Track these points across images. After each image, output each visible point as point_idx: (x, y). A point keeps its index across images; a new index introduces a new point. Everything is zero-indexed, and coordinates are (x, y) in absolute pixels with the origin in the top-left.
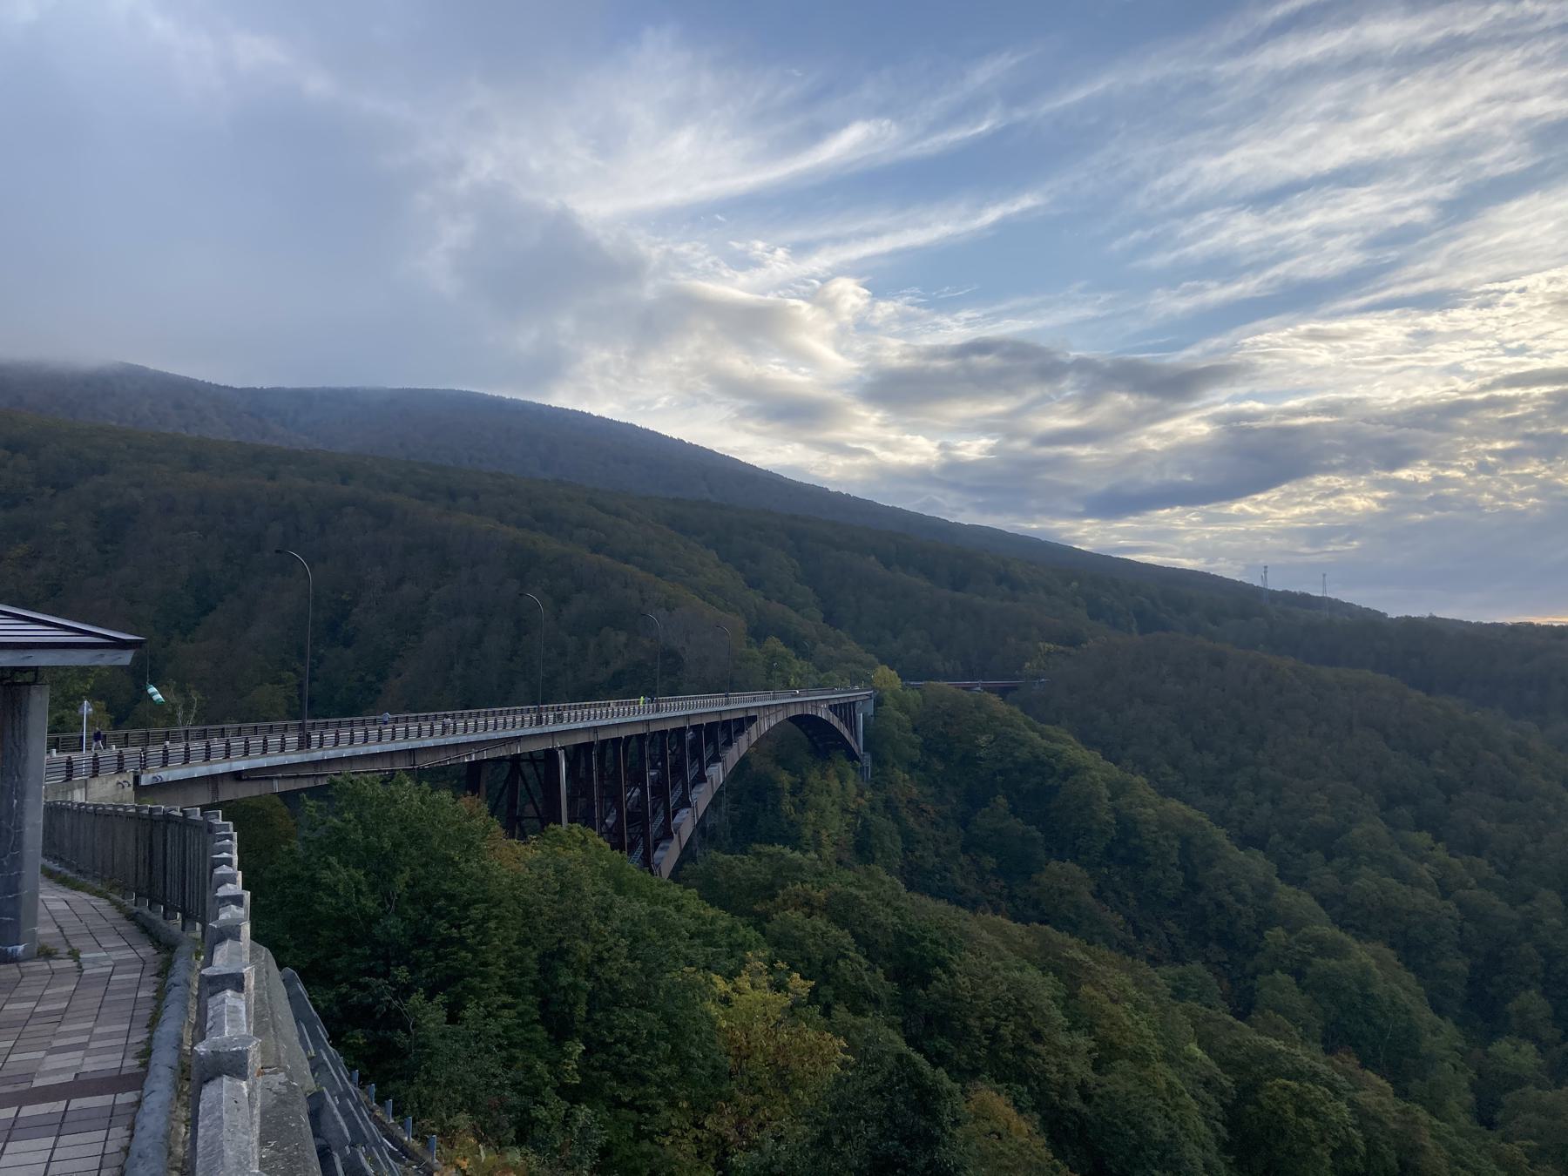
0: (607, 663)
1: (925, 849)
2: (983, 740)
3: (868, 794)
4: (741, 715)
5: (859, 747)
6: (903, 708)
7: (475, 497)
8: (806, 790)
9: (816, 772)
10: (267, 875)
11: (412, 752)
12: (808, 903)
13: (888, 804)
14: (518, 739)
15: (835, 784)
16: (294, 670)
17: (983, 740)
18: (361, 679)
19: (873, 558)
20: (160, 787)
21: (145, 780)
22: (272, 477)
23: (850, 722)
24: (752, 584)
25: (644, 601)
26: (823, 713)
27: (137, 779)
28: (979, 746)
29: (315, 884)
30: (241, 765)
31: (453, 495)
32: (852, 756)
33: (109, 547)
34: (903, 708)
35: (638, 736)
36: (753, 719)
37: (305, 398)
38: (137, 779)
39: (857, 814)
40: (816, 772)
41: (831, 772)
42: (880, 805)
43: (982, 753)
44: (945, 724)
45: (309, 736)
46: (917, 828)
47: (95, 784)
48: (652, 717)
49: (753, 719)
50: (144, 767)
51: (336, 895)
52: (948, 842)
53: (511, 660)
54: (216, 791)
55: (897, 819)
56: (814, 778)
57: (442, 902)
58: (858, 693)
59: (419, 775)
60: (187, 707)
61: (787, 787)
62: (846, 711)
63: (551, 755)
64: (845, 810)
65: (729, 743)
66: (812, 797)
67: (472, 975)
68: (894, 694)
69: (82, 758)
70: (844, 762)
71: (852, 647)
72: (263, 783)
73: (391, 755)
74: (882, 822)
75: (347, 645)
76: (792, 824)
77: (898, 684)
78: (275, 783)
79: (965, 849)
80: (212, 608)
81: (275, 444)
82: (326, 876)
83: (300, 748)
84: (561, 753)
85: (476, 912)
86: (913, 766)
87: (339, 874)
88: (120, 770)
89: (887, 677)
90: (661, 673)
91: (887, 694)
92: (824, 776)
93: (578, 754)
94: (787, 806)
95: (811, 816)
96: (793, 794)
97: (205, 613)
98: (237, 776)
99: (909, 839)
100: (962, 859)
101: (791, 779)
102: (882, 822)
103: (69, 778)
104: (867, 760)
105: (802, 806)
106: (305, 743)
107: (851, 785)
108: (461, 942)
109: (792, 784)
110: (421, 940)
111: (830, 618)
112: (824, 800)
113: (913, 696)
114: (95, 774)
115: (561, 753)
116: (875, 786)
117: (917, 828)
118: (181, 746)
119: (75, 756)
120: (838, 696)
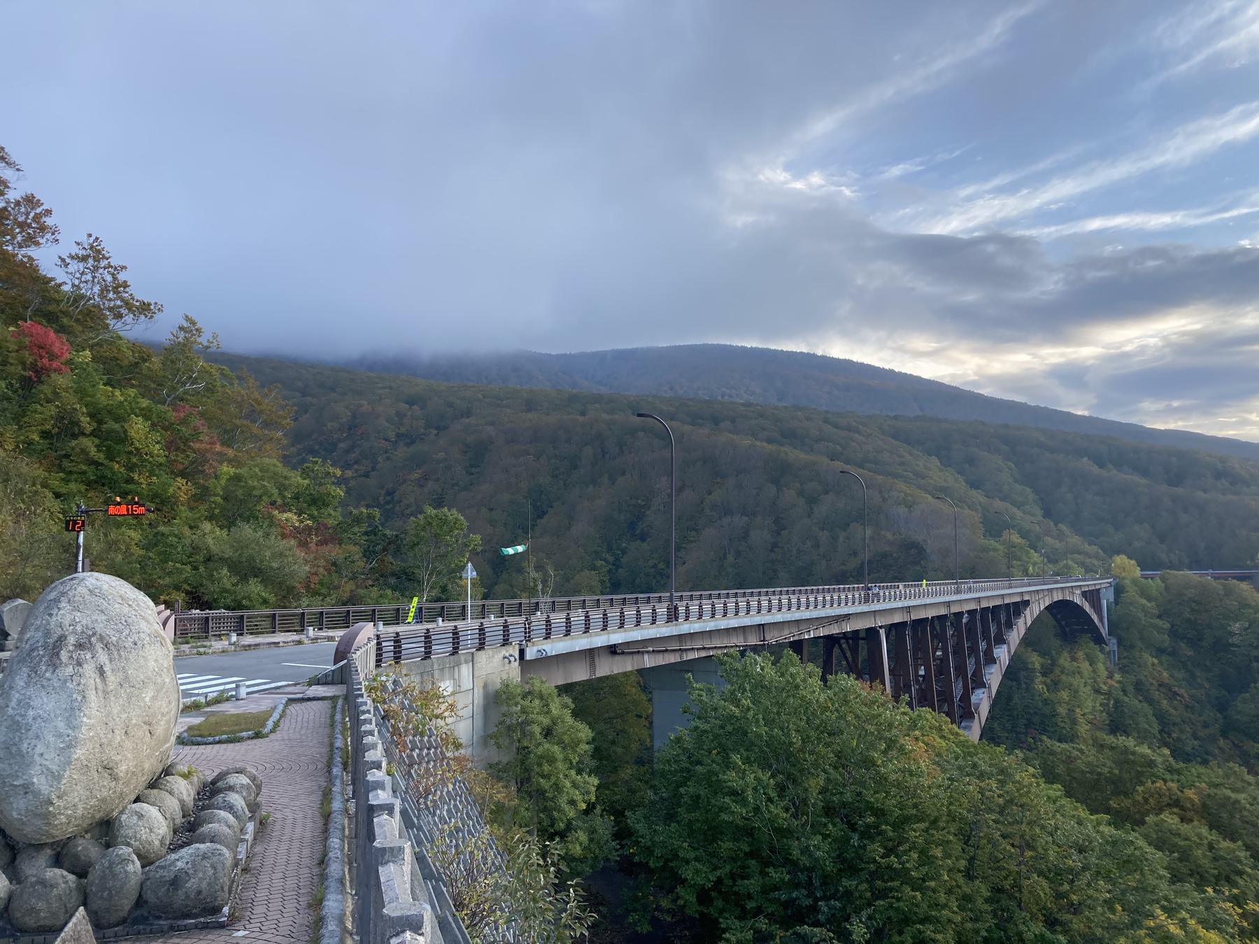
0: (855, 554)
1: (1182, 732)
2: (1236, 627)
3: (1117, 677)
4: (1018, 599)
5: (1104, 631)
6: (1143, 593)
7: (733, 421)
8: (1057, 671)
9: (1066, 654)
10: (869, 894)
11: (761, 627)
12: (1176, 803)
13: (1138, 686)
14: (847, 617)
15: (1085, 666)
16: (605, 560)
17: (1236, 627)
18: (655, 566)
19: (1085, 459)
20: (546, 661)
21: (530, 654)
22: (583, 414)
23: (1097, 607)
24: (975, 485)
25: (884, 500)
26: (1078, 600)
27: (522, 652)
28: (1232, 634)
29: (717, 787)
30: (617, 638)
31: (716, 421)
32: (1099, 640)
33: (473, 470)
34: (1143, 593)
35: (939, 617)
36: (1027, 603)
37: (600, 358)
38: (522, 652)
39: (1108, 694)
40: (1066, 654)
41: (1080, 654)
42: (1130, 688)
43: (1235, 640)
44: (1193, 610)
45: (676, 608)
46: (1173, 711)
47: (482, 657)
48: (954, 598)
49: (1027, 603)
50: (528, 639)
51: (744, 802)
52: (1206, 725)
53: (772, 551)
54: (593, 666)
55: (1150, 701)
56: (1064, 660)
57: (870, 820)
58: (1103, 583)
59: (776, 651)
60: (544, 582)
61: (1037, 666)
62: (1092, 596)
63: (872, 633)
64: (1097, 691)
65: (1010, 625)
66: (1064, 677)
67: (922, 921)
68: (1134, 582)
69: (469, 625)
70: (1092, 644)
71: (1075, 540)
72: (636, 657)
73: (743, 629)
74: (1133, 702)
75: (643, 540)
76: (1045, 702)
77: (1138, 572)
78: (646, 657)
79: (1224, 734)
80: (544, 513)
81: (309, 824)
82: (731, 778)
83: (669, 620)
84: (882, 632)
85: (915, 832)
86: (1160, 651)
87: (746, 777)
88: (506, 642)
89: (1126, 566)
90: (905, 564)
91: (1127, 581)
92: (1074, 659)
93: (896, 630)
94: (1039, 685)
95: (1064, 695)
96: (1044, 674)
97: (540, 517)
98: (613, 650)
99: (1161, 717)
100: (1222, 742)
101: (1042, 660)
102: (1133, 702)
103: (455, 651)
104: (1112, 645)
105: (1055, 686)
106: (673, 616)
107: (1101, 666)
108: (903, 876)
109: (1042, 666)
110: (849, 867)
111: (1047, 514)
112: (1076, 681)
113: (1155, 585)
114: (481, 647)
115: (882, 632)
116: (1123, 670)
117: (1173, 711)
118: (564, 615)
119: (460, 624)
120: (1090, 584)
